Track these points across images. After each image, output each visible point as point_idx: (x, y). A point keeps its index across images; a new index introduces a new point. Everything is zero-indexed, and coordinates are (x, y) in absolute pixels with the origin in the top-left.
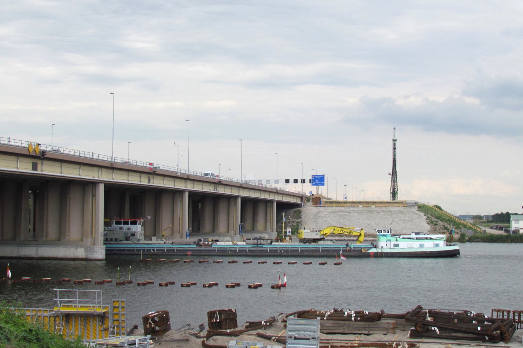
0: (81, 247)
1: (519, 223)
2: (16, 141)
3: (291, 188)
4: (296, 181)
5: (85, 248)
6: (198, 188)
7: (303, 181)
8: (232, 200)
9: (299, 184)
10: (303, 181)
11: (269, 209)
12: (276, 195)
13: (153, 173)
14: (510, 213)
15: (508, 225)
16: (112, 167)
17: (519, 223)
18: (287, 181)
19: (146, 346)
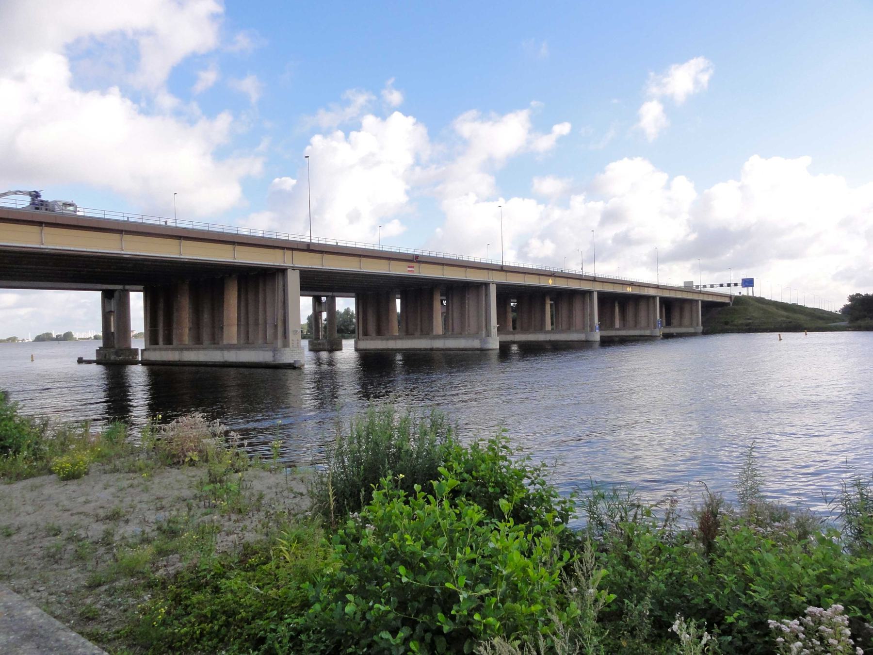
0: (477, 338)
1: (685, 282)
2: (106, 213)
3: (725, 290)
4: (729, 285)
5: (480, 340)
6: (667, 294)
7: (736, 285)
8: (651, 300)
9: (732, 287)
10: (736, 285)
11: (651, 305)
12: (416, 265)
13: (415, 259)
14: (755, 159)
15: (467, 581)
16: (309, 248)
17: (685, 282)
18: (721, 285)
19: (18, 654)
